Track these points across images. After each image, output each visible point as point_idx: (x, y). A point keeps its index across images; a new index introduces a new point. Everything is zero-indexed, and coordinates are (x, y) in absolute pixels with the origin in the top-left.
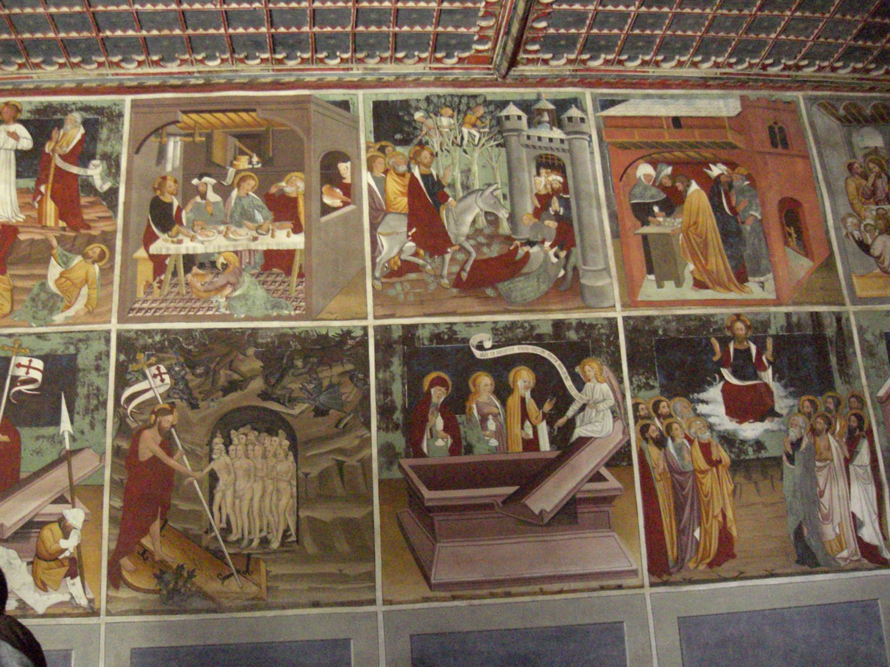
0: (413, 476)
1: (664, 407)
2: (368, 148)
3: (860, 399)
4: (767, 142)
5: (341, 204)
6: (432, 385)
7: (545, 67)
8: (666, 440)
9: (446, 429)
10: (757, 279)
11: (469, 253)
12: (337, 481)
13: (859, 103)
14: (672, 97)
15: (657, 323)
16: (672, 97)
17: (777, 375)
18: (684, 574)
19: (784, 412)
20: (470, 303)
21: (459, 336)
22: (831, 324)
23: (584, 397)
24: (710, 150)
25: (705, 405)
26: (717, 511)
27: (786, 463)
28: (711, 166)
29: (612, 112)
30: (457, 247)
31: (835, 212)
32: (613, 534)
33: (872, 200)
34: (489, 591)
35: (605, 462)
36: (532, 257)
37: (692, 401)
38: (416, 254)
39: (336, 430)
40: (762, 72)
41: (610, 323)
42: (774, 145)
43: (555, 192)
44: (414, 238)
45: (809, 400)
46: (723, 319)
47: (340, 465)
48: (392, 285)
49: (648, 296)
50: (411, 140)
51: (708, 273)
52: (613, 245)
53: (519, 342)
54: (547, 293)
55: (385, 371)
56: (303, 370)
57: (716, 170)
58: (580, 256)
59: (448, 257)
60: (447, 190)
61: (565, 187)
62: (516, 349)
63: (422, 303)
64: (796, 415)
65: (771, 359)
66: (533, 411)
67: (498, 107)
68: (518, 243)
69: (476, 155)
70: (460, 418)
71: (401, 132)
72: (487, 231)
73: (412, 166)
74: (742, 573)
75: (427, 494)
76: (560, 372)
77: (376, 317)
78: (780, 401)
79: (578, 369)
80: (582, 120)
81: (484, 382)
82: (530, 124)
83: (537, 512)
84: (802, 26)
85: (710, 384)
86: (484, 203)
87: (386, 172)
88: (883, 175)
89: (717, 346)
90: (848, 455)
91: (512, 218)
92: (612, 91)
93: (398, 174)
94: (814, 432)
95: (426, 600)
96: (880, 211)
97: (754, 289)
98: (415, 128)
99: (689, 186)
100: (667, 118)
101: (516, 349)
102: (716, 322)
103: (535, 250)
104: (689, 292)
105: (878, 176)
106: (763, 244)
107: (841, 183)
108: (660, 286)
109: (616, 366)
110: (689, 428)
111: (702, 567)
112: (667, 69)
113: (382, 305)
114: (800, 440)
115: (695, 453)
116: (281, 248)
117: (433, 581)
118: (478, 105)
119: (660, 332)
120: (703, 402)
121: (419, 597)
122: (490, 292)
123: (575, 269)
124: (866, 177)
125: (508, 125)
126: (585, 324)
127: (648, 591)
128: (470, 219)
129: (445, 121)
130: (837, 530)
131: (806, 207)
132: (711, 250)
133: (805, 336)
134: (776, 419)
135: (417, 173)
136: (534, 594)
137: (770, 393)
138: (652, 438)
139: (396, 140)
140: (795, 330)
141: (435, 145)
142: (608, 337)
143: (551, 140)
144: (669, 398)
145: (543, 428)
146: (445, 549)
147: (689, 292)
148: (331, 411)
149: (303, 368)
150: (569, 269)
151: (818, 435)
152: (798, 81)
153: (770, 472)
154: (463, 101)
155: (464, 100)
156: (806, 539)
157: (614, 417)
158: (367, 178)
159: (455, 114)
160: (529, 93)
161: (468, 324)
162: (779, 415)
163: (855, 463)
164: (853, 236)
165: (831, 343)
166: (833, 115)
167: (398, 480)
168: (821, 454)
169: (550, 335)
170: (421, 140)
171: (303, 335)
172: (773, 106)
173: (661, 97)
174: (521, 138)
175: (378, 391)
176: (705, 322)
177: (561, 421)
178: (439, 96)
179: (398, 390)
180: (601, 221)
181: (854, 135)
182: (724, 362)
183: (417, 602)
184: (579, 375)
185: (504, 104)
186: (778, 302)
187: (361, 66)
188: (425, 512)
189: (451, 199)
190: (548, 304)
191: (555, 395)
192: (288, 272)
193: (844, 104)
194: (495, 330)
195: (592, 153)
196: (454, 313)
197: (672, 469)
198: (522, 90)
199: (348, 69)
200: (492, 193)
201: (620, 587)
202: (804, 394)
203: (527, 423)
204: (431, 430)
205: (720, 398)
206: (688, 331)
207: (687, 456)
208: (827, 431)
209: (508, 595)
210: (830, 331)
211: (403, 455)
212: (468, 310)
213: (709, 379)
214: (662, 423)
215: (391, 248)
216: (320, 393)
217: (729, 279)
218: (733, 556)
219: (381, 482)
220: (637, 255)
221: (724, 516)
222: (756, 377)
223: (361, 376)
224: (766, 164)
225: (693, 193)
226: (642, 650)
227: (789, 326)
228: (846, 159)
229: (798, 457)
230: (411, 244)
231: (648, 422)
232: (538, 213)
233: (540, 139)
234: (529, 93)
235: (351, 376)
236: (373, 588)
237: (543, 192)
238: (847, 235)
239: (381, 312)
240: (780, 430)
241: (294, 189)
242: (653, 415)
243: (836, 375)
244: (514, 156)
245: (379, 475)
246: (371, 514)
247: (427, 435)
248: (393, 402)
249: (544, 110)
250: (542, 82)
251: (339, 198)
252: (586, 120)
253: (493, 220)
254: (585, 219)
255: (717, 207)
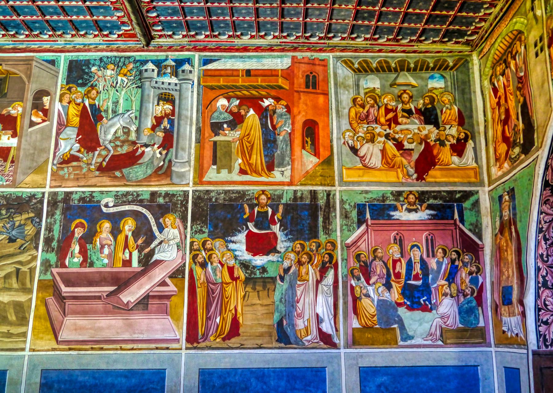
0: (58, 278)
1: (209, 244)
2: (62, 88)
3: (334, 245)
4: (303, 86)
5: (41, 121)
6: (76, 227)
7: (171, 40)
8: (207, 264)
9: (80, 253)
10: (280, 169)
11: (110, 151)
12: (14, 280)
13: (389, 60)
14: (249, 57)
15: (213, 194)
16: (249, 57)
17: (283, 228)
18: (207, 343)
19: (282, 250)
20: (106, 180)
21: (95, 199)
22: (323, 198)
23: (162, 236)
24: (266, 90)
25: (234, 244)
26: (232, 307)
27: (279, 281)
28: (264, 99)
29: (210, 67)
30: (103, 147)
31: (339, 128)
32: (169, 317)
33: (365, 121)
34: (91, 346)
35: (169, 275)
36: (146, 154)
37: (227, 241)
38: (79, 151)
39: (19, 251)
40: (306, 41)
41: (184, 194)
42: (307, 87)
43: (167, 115)
44: (79, 142)
45: (300, 244)
46: (253, 193)
47: (18, 270)
48: (62, 169)
49: (210, 178)
50: (87, 84)
51: (250, 165)
52: (196, 147)
53: (129, 203)
54: (150, 175)
55: (51, 218)
56: (6, 216)
57: (267, 103)
58: (174, 153)
59: (97, 153)
60: (103, 114)
61: (173, 113)
62: (127, 208)
63: (78, 179)
64: (289, 252)
65: (280, 218)
66: (131, 244)
67: (142, 63)
68: (139, 145)
69: (123, 93)
70: (89, 246)
71: (82, 79)
72: (122, 138)
73: (85, 99)
74: (242, 345)
75: (64, 289)
76: (151, 222)
77: (51, 187)
78: (281, 244)
79: (161, 220)
80: (191, 72)
81: (107, 225)
82: (159, 74)
83: (125, 302)
84: (317, 12)
85: (240, 232)
86: (123, 121)
87: (69, 103)
88: (375, 105)
89: (247, 210)
90: (319, 279)
91: (138, 131)
92: (212, 54)
93: (76, 104)
94: (300, 263)
95: (54, 350)
96: (370, 128)
97: (277, 175)
98: (91, 77)
99: (248, 112)
100: (243, 70)
101: (127, 208)
102: (249, 195)
103: (149, 149)
104: (235, 176)
105: (372, 106)
106: (289, 148)
107: (346, 111)
108: (218, 172)
109: (184, 219)
110: (223, 257)
111: (218, 340)
112: (245, 40)
113: (55, 180)
114: (289, 268)
115: (224, 272)
116: (3, 146)
117: (59, 339)
118: (130, 62)
119: (214, 200)
120: (233, 242)
121: (50, 348)
122: (118, 174)
123: (170, 161)
124: (363, 106)
125: (145, 75)
126: (169, 194)
127: (184, 352)
128: (113, 130)
129: (109, 72)
130: (306, 323)
131: (321, 125)
132: (254, 151)
133: (305, 205)
134: (276, 254)
135: (87, 104)
136: (117, 349)
137: (276, 238)
138: (199, 262)
139: (78, 84)
140: (299, 201)
141: (101, 87)
142: (182, 202)
143: (169, 84)
144: (213, 239)
145: (135, 254)
146: (69, 321)
147: (235, 176)
148: (18, 240)
149: (6, 215)
150: (167, 161)
151: (302, 265)
152: (331, 46)
153: (268, 286)
154: (121, 60)
155: (122, 60)
156: (284, 327)
157: (178, 249)
158: (58, 106)
159: (116, 68)
160: (161, 55)
161: (102, 193)
162: (279, 252)
163: (323, 283)
164: (348, 144)
165: (321, 208)
166: (350, 67)
167: (49, 280)
168: (302, 276)
169: (147, 200)
170: (93, 84)
171: (8, 196)
172: (312, 62)
173: (241, 57)
174: (152, 82)
175: (46, 230)
176: (242, 195)
177: (147, 250)
178: (108, 57)
179: (57, 229)
180: (191, 132)
181: (361, 80)
182: (250, 219)
183: (48, 350)
184: (161, 224)
185: (146, 62)
186: (291, 184)
187: (63, 39)
188: (61, 299)
189: (104, 119)
190: (149, 181)
191: (146, 234)
192: (5, 160)
193: (359, 60)
194: (116, 196)
195: (192, 92)
196: (95, 186)
197: (208, 281)
198: (158, 53)
199: (55, 41)
200: (129, 115)
201: (167, 348)
202: (297, 239)
203: (127, 251)
204: (72, 252)
205: (244, 241)
206: (231, 200)
207: (219, 274)
208: (308, 262)
209: (102, 349)
210: (322, 202)
211: (54, 266)
212: (103, 184)
213: (239, 228)
214: (206, 254)
215: (66, 147)
216: (13, 229)
217: (263, 169)
218: (238, 335)
219: (39, 281)
220: (208, 153)
221: (236, 310)
222: (269, 228)
223: (38, 220)
224: (300, 98)
225: (250, 116)
226: (175, 386)
227: (295, 199)
228: (352, 95)
229: (287, 278)
230: (78, 145)
231: (198, 252)
232: (153, 128)
233: (163, 83)
234: (161, 55)
235: (32, 219)
236: (25, 342)
237: (159, 115)
238: (344, 143)
239: (54, 184)
240: (278, 261)
241: (16, 111)
242: (202, 249)
243: (321, 229)
244: (146, 92)
245: (39, 277)
246: (31, 299)
247: (69, 255)
248: (53, 235)
249: (168, 66)
250: (170, 48)
251: (41, 117)
252: (193, 72)
253: (127, 132)
254: (182, 130)
255: (264, 126)
